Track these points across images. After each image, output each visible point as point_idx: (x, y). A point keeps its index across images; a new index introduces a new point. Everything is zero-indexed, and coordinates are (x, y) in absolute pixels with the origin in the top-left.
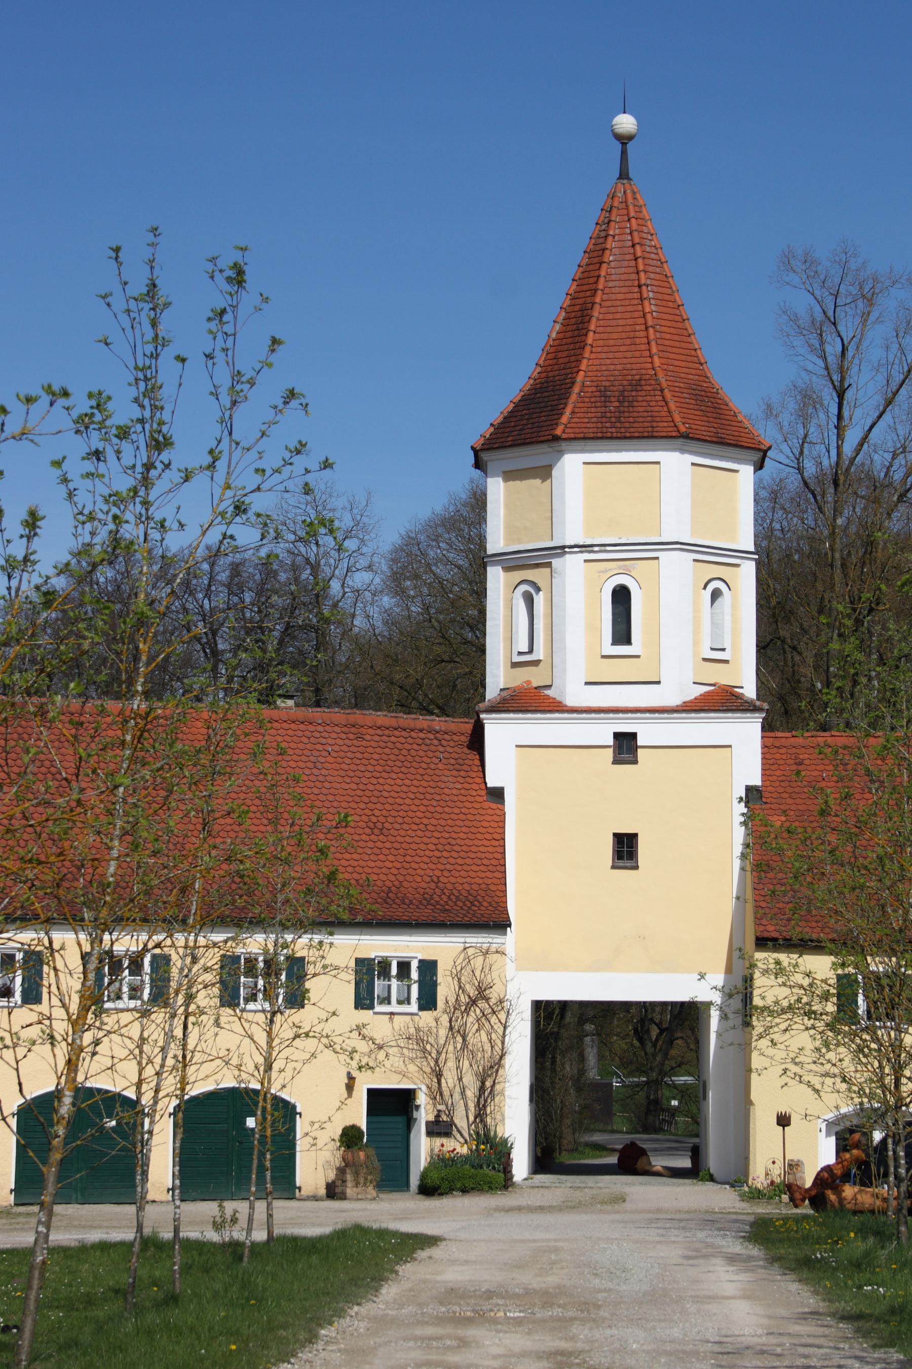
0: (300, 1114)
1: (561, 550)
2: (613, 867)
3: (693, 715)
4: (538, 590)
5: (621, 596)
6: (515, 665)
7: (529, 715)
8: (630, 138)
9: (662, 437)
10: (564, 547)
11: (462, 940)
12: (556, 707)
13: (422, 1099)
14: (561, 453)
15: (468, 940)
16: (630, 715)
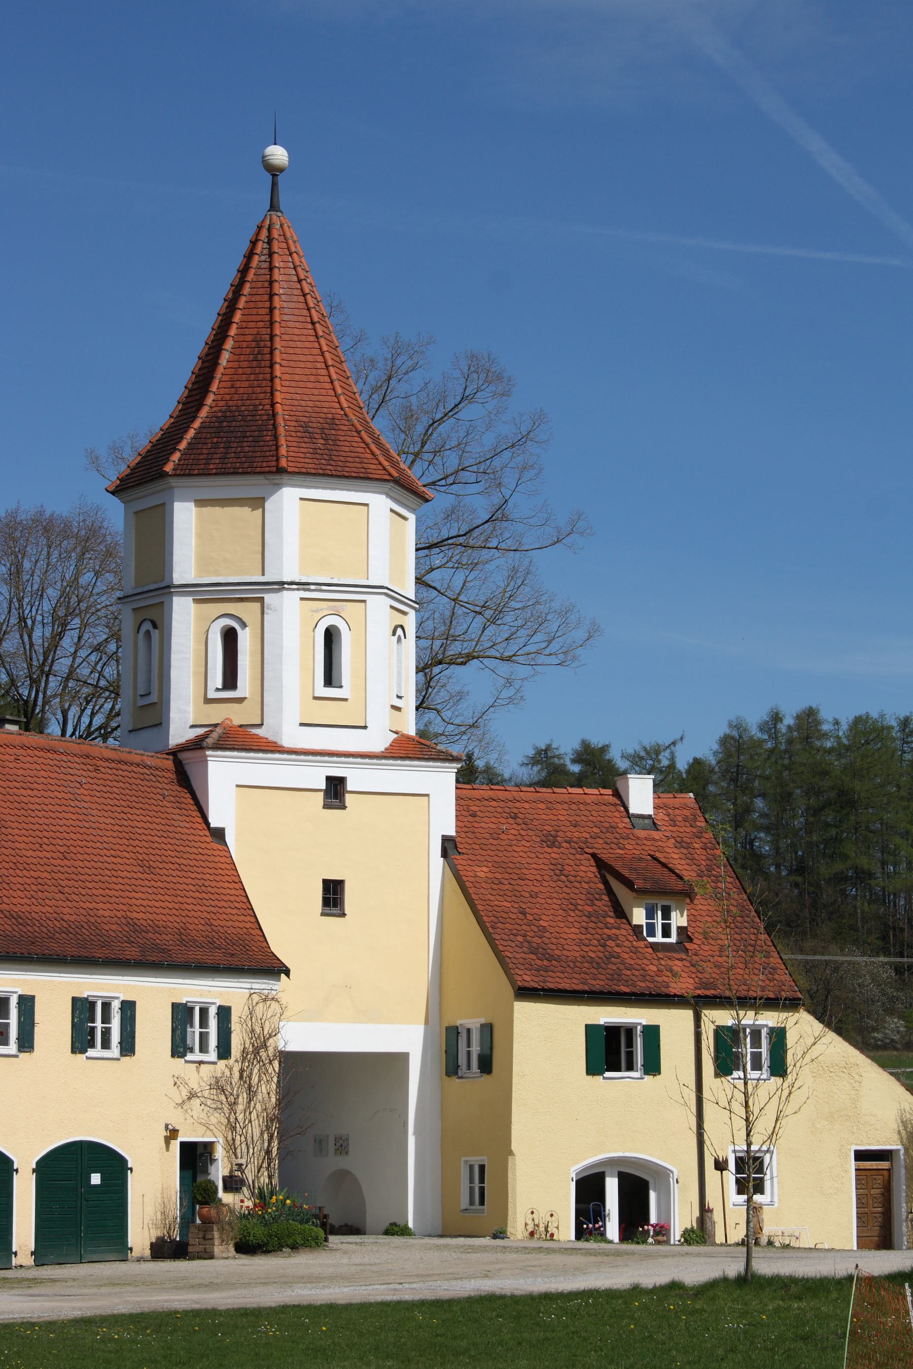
0: (131, 1169)
1: (281, 585)
2: (323, 914)
3: (399, 762)
4: (244, 625)
5: (331, 637)
6: (208, 701)
7: (252, 755)
8: (281, 170)
9: (377, 479)
10: (283, 583)
11: (249, 986)
12: (271, 748)
13: (220, 1153)
14: (279, 486)
15: (254, 986)
16: (318, 758)
